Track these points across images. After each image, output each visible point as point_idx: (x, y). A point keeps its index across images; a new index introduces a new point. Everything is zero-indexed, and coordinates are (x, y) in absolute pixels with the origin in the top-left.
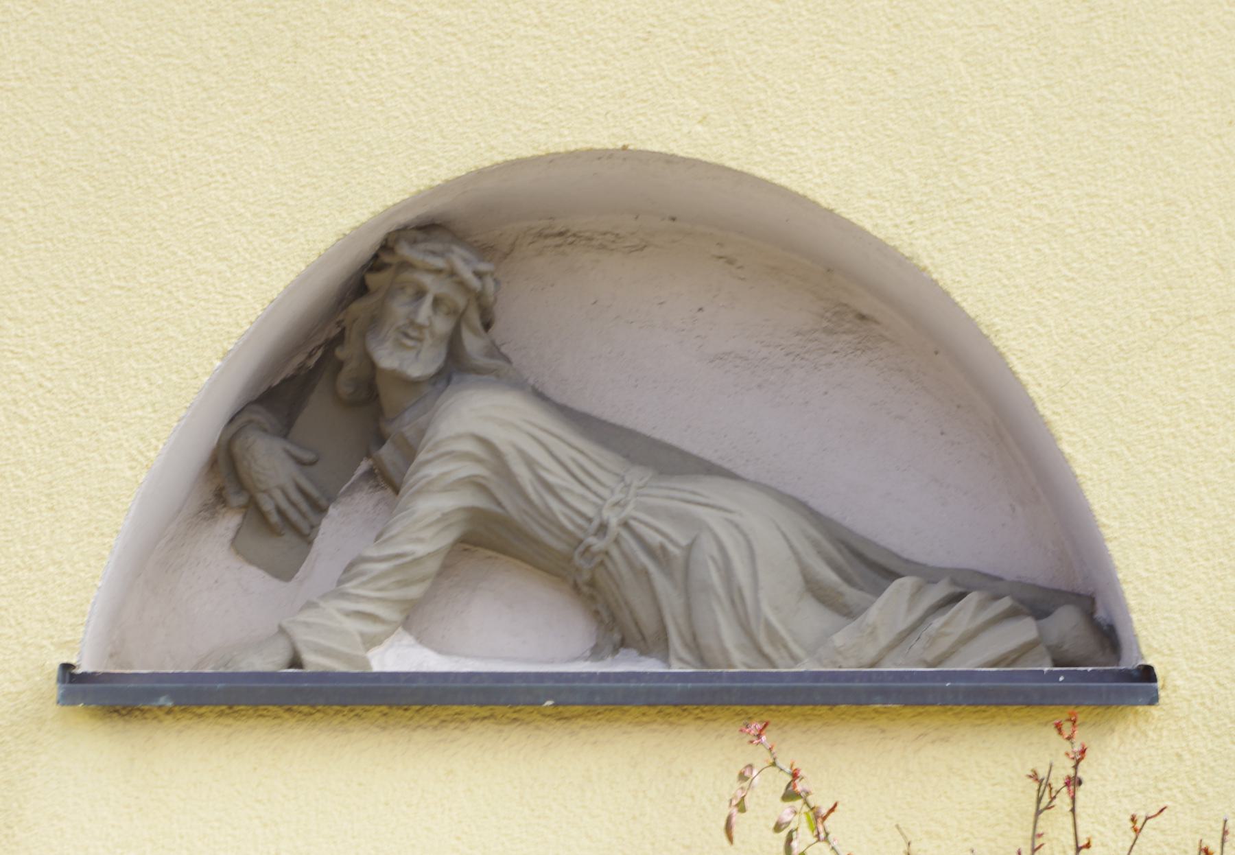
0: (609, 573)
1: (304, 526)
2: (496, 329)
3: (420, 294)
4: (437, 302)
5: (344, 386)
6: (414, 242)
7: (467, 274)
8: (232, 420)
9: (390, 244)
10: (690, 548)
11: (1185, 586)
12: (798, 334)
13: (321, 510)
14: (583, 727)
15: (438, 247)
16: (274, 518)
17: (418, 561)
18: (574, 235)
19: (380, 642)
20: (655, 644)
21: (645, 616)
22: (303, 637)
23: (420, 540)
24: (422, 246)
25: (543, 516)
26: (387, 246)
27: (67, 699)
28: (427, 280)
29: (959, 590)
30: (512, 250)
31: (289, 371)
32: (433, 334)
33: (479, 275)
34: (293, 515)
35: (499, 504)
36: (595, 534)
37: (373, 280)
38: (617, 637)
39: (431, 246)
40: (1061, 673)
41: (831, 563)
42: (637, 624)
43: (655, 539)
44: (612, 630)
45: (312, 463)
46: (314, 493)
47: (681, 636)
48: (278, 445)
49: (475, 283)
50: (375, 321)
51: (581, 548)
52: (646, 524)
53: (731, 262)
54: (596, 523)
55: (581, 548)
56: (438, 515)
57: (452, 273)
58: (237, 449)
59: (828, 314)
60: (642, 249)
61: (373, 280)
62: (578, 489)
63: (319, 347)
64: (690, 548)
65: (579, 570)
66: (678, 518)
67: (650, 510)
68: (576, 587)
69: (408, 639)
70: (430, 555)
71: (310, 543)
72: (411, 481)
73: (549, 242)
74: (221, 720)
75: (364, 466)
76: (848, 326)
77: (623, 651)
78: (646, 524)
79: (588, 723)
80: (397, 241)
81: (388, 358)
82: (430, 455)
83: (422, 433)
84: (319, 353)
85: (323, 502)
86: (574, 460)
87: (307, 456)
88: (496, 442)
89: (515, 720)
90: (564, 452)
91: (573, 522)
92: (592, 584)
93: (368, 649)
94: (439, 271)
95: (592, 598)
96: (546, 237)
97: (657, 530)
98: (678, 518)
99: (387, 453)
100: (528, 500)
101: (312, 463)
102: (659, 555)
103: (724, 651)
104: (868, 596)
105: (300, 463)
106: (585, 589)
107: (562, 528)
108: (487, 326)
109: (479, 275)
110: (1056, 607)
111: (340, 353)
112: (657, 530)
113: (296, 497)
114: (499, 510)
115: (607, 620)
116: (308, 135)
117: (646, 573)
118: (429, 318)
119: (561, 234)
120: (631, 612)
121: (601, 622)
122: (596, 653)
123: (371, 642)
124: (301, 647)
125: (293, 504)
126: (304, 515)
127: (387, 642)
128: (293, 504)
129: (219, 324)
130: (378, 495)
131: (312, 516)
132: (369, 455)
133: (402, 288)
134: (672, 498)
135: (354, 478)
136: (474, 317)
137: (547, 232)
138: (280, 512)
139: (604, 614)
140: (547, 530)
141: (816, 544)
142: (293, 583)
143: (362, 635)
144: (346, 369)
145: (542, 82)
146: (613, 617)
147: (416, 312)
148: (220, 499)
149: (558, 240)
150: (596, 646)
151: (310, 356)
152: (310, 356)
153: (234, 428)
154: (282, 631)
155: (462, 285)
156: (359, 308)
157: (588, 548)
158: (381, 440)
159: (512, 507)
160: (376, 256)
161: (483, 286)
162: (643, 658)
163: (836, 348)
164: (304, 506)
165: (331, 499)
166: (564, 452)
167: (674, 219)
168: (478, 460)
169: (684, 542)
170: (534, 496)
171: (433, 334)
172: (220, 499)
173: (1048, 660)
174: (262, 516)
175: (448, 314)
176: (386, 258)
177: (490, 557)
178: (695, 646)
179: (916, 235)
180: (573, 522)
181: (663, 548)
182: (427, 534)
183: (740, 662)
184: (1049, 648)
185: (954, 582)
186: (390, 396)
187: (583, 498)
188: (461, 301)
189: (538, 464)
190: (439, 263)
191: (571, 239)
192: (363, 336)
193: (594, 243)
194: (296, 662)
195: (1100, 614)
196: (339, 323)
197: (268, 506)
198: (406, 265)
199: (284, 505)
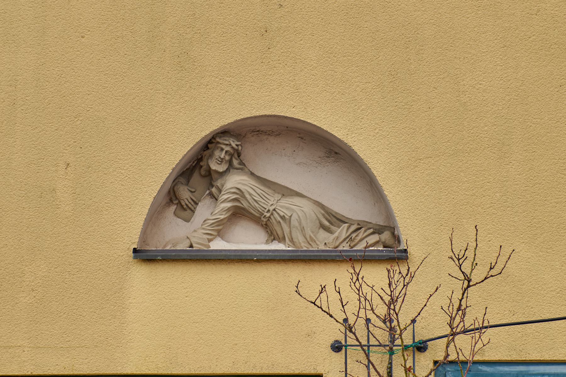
0: (271, 222)
1: (193, 208)
2: (241, 157)
3: (222, 149)
4: (226, 152)
5: (203, 172)
6: (220, 137)
7: (234, 145)
8: (174, 181)
9: (214, 137)
10: (291, 216)
11: (416, 228)
12: (320, 157)
13: (197, 204)
14: (264, 264)
15: (227, 139)
16: (185, 207)
17: (222, 220)
18: (262, 131)
19: (212, 240)
20: (281, 239)
21: (280, 233)
22: (193, 240)
23: (222, 215)
24: (223, 138)
25: (254, 208)
26: (213, 138)
27: (135, 258)
28: (223, 147)
29: (360, 226)
30: (245, 136)
31: (188, 167)
32: (225, 160)
33: (237, 145)
34: (190, 206)
35: (242, 204)
36: (267, 213)
37: (210, 146)
38: (273, 238)
39: (225, 138)
40: (385, 250)
41: (327, 219)
42: (278, 235)
43: (282, 214)
44: (271, 236)
45: (194, 192)
46: (195, 200)
47: (289, 239)
48: (186, 188)
49: (236, 147)
50: (211, 156)
51: (263, 216)
52: (280, 210)
53: (302, 138)
54: (267, 209)
55: (263, 216)
56: (227, 208)
57: (230, 145)
58: (175, 189)
59: (327, 152)
60: (279, 135)
61: (210, 146)
62: (261, 200)
63: (196, 160)
64: (291, 216)
65: (263, 221)
66: (287, 208)
67: (281, 207)
68: (262, 225)
69: (219, 239)
70: (225, 218)
71: (194, 212)
72: (220, 199)
73: (255, 133)
74: (173, 262)
75: (208, 192)
76: (332, 155)
77: (274, 241)
78: (280, 210)
79: (265, 263)
80: (216, 137)
81: (214, 166)
82: (225, 193)
83: (223, 186)
84: (196, 162)
85: (197, 202)
86: (262, 193)
87: (193, 190)
88: (242, 189)
89: (247, 262)
90: (259, 191)
91: (261, 209)
92: (266, 225)
93: (209, 242)
94: (227, 145)
95: (266, 228)
96: (254, 132)
97: (283, 212)
98: (287, 208)
99: (214, 190)
100: (249, 203)
101: (194, 192)
102: (283, 218)
103: (300, 243)
104: (337, 228)
105: (191, 192)
106: (264, 226)
107: (258, 211)
108: (239, 156)
109: (237, 145)
110: (385, 231)
111: (202, 164)
112: (283, 212)
113: (190, 201)
114: (242, 206)
115: (270, 233)
116: (194, 111)
117: (280, 222)
118: (224, 156)
119: (258, 131)
120: (276, 232)
121: (269, 233)
122: (267, 242)
123: (210, 240)
124: (192, 242)
125: (190, 203)
126: (192, 205)
127: (214, 240)
128: (190, 203)
129: (171, 160)
130: (211, 200)
131: (195, 206)
132: (209, 189)
133: (218, 148)
134: (287, 203)
135: (205, 195)
136: (236, 155)
137: (255, 130)
138: (186, 205)
139: (269, 232)
140: (254, 211)
141: (323, 215)
142: (190, 223)
143: (208, 239)
144: (203, 168)
145: (253, 97)
146: (272, 233)
147: (221, 155)
148: (171, 201)
149: (257, 133)
150: (267, 239)
151: (194, 162)
152: (194, 162)
153: (175, 183)
154: (188, 238)
155: (232, 148)
156: (207, 153)
157: (265, 216)
158: (213, 186)
159: (245, 205)
160: (211, 140)
161: (238, 148)
162: (279, 243)
163: (329, 161)
164: (193, 203)
165: (199, 201)
166: (259, 191)
167: (287, 127)
168: (237, 194)
169: (290, 215)
170: (252, 204)
171: (225, 160)
172: (171, 201)
173: (382, 246)
174: (182, 206)
175: (229, 155)
176: (213, 141)
177: (240, 217)
178: (292, 240)
179: (348, 137)
180: (261, 209)
181: (284, 216)
182: (224, 213)
183: (304, 247)
184: (382, 242)
185: (358, 224)
186: (214, 176)
187: (264, 203)
188: (232, 151)
189: (253, 195)
190: (227, 143)
191: (261, 133)
192: (208, 159)
193: (267, 133)
194: (191, 246)
195: (396, 233)
196: (201, 155)
197: (183, 204)
198: (218, 143)
199: (187, 203)
